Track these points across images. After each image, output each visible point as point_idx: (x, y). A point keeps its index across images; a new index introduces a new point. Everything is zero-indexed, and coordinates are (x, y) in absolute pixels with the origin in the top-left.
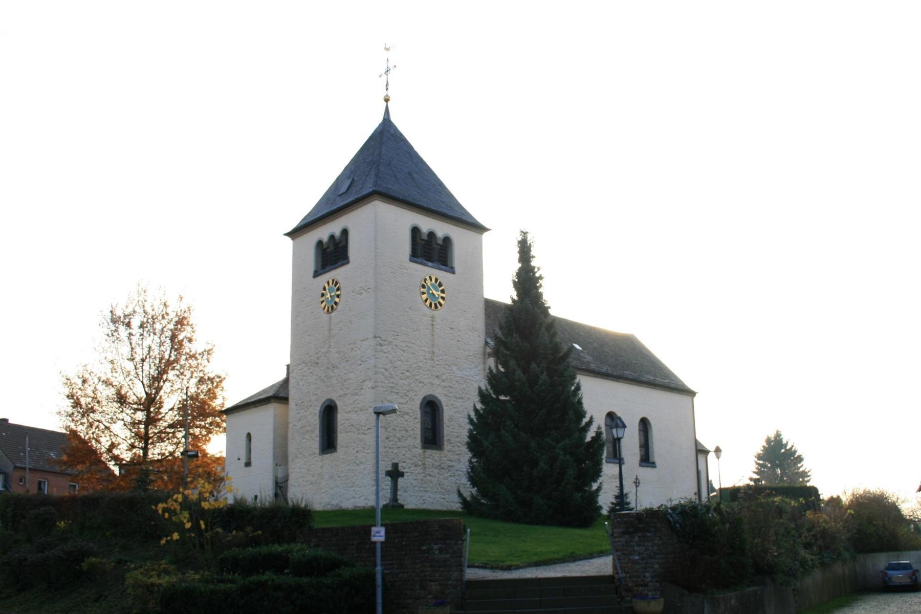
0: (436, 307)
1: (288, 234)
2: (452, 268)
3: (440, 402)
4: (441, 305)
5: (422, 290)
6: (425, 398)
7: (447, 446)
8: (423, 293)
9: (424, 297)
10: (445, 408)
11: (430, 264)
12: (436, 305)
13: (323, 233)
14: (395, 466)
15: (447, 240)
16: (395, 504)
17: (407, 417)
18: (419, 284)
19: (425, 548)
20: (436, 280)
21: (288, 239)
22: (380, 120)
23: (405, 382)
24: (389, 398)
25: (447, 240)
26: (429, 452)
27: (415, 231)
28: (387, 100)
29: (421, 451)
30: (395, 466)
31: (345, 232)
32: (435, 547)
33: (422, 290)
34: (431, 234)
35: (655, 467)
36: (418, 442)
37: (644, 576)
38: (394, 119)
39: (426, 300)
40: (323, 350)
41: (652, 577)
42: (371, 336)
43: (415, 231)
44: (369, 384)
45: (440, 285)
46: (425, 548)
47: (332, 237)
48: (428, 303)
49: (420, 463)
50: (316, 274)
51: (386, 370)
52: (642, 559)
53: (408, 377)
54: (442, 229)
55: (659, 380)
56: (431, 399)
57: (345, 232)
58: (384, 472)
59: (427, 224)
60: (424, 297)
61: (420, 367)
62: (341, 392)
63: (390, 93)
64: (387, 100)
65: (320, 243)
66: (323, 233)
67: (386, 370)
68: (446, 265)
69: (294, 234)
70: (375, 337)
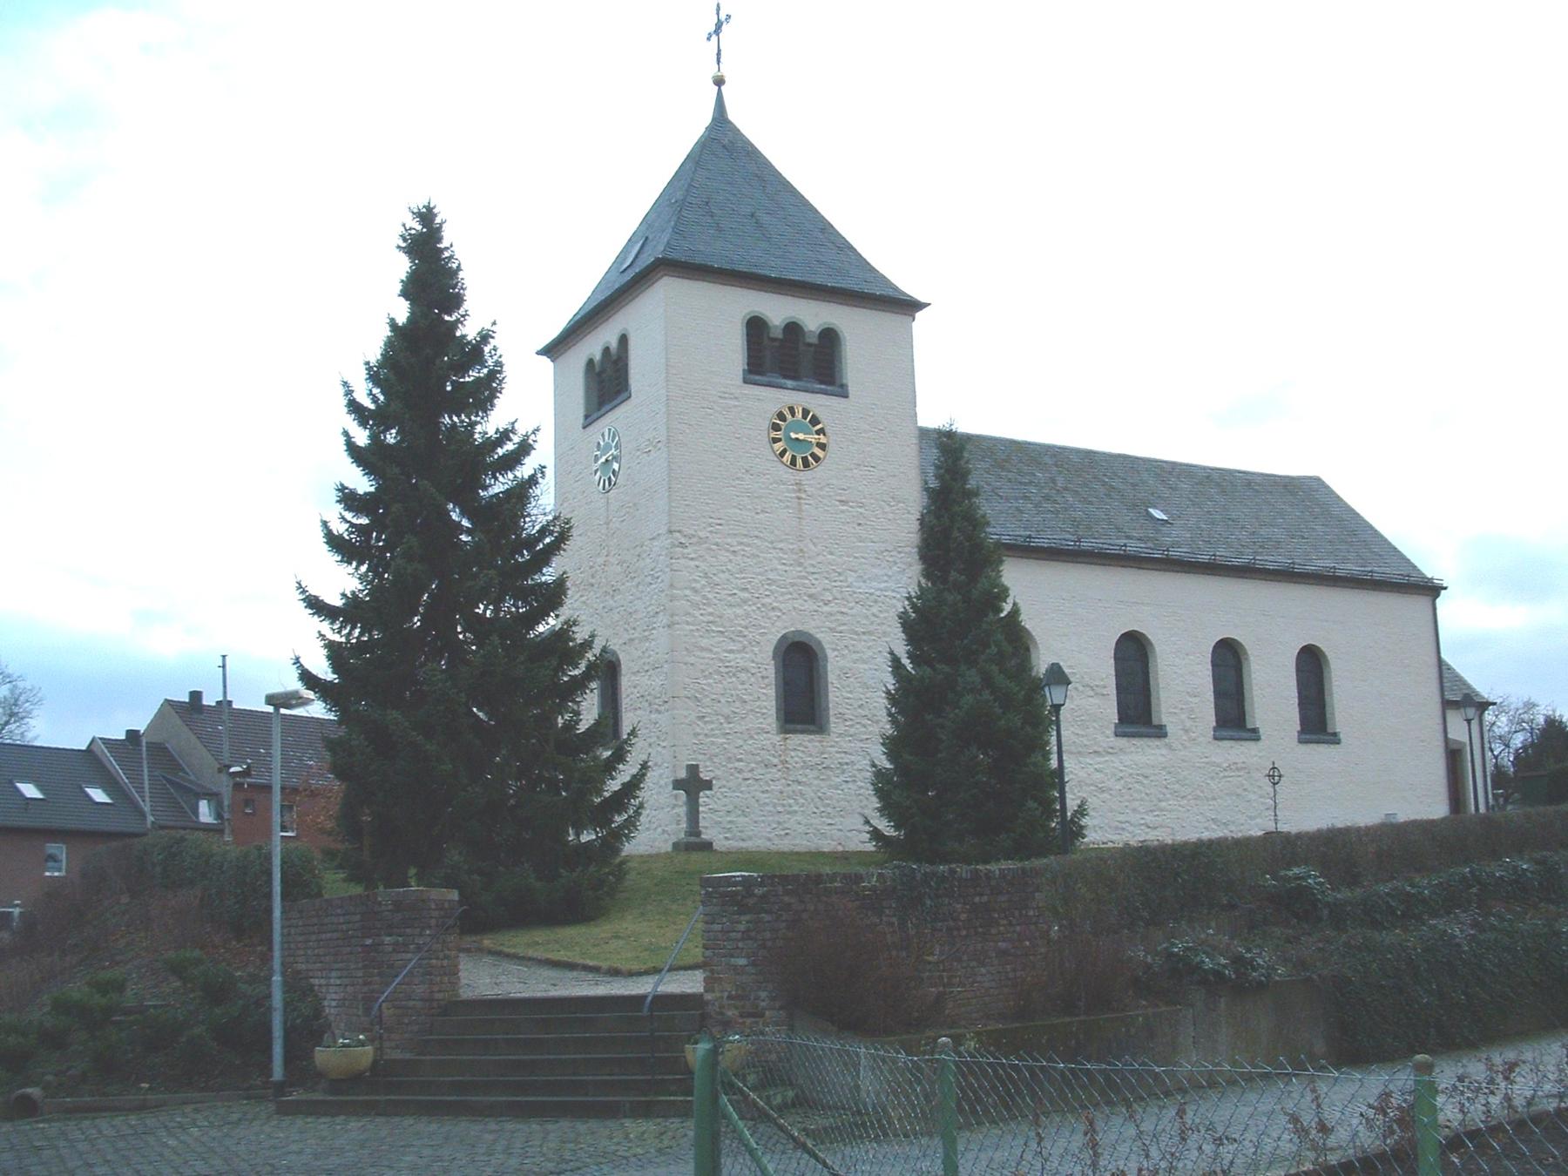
0: (806, 464)
1: (541, 352)
2: (843, 386)
3: (819, 643)
4: (817, 459)
5: (773, 434)
6: (784, 637)
7: (835, 725)
8: (775, 440)
9: (779, 447)
10: (830, 654)
11: (790, 383)
12: (805, 460)
13: (594, 345)
14: (693, 770)
15: (830, 338)
16: (692, 839)
17: (743, 676)
18: (766, 424)
19: (369, 942)
20: (805, 412)
21: (545, 360)
22: (706, 118)
23: (739, 611)
24: (704, 642)
25: (830, 338)
26: (796, 739)
27: (755, 327)
28: (719, 82)
29: (777, 738)
30: (693, 770)
31: (623, 340)
32: (387, 939)
33: (773, 434)
34: (793, 328)
35: (1338, 742)
36: (771, 720)
37: (757, 998)
38: (733, 115)
39: (784, 451)
40: (600, 560)
41: (773, 999)
42: (663, 530)
43: (755, 327)
44: (663, 619)
45: (815, 421)
46: (369, 942)
47: (606, 350)
48: (788, 457)
49: (775, 761)
50: (589, 419)
51: (695, 591)
52: (754, 964)
53: (745, 601)
54: (813, 316)
55: (1379, 570)
56: (802, 639)
57: (623, 340)
58: (667, 780)
59: (778, 310)
60: (779, 447)
61: (772, 582)
62: (626, 637)
63: (725, 71)
64: (719, 82)
65: (590, 362)
66: (594, 345)
67: (695, 591)
68: (831, 382)
69: (552, 350)
70: (671, 532)
